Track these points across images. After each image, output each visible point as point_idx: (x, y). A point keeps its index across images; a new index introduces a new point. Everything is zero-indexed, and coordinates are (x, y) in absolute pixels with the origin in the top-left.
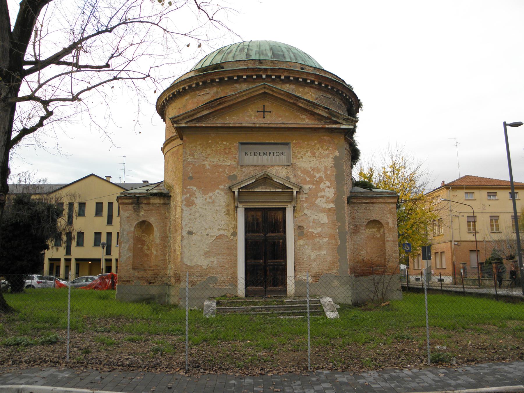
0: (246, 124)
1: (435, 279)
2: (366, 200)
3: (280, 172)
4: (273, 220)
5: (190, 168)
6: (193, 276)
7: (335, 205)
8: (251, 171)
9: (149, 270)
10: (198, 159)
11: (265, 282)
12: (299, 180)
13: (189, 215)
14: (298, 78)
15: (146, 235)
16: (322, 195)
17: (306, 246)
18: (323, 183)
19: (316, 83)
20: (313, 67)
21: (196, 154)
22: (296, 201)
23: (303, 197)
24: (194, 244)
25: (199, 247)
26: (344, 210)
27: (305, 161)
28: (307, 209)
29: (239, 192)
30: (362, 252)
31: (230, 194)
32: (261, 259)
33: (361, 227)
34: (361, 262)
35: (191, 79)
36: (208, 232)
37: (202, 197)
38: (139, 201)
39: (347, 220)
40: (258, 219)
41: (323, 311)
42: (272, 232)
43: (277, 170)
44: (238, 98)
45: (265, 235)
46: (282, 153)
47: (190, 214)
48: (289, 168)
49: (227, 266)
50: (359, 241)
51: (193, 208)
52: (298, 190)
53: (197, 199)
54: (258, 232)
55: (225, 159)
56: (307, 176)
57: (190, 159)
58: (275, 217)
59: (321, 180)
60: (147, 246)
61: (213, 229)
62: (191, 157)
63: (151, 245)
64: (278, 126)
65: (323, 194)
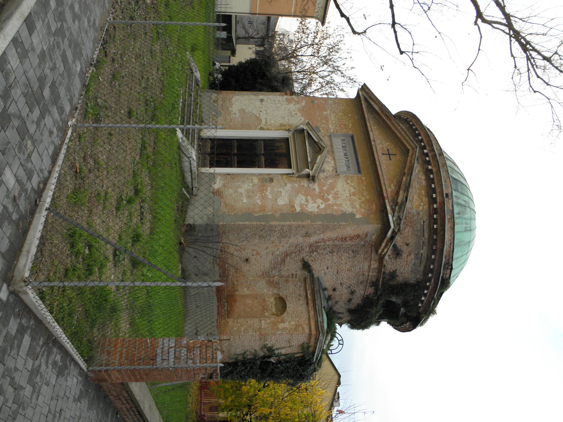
1: (219, 6)
2: (310, 295)
6: (222, 102)
7: (299, 212)
12: (322, 181)
17: (251, 185)
18: (323, 202)
20: (453, 210)
25: (250, 106)
30: (245, 289)
32: (238, 150)
33: (276, 289)
34: (233, 287)
42: (265, 161)
44: (397, 129)
45: (263, 154)
46: (349, 167)
48: (334, 172)
50: (259, 286)
54: (265, 150)
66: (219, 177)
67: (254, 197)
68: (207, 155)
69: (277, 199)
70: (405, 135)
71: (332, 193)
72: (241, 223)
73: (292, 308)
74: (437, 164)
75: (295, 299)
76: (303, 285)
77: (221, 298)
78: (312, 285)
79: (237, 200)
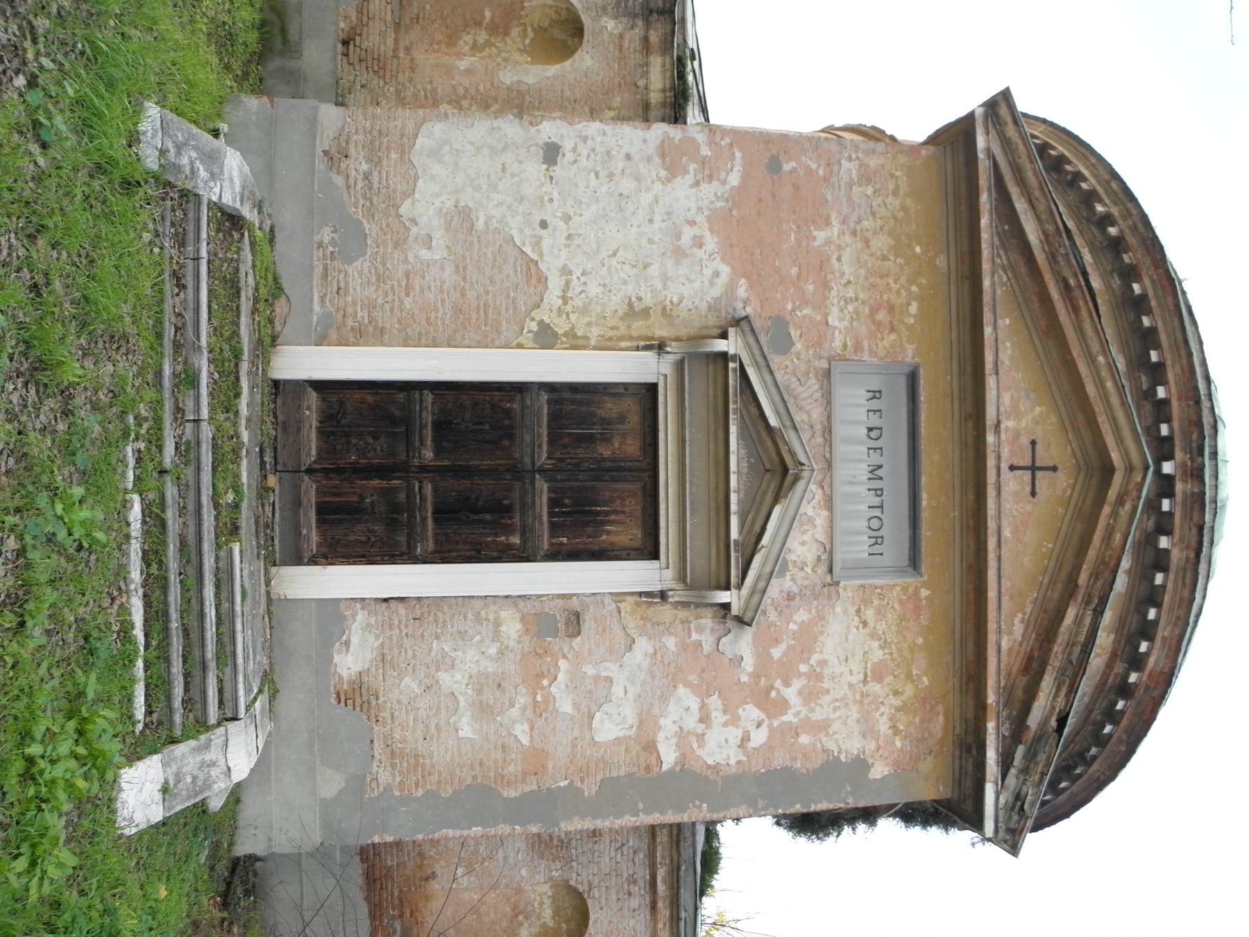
0: (994, 392)
2: (664, 882)
3: (804, 533)
4: (605, 503)
5: (814, 166)
6: (369, 160)
7: (671, 772)
8: (808, 412)
9: (396, 40)
10: (849, 198)
11: (339, 470)
12: (773, 616)
13: (625, 150)
14: (1158, 605)
15: (527, 41)
16: (714, 714)
17: (493, 651)
18: (763, 716)
19: (1133, 678)
21: (870, 191)
22: (685, 605)
23: (704, 631)
24: (504, 169)
25: (494, 187)
26: (647, 813)
27: (851, 637)
28: (651, 651)
29: (724, 356)
31: (712, 320)
32: (439, 450)
33: (559, 865)
34: (420, 867)
35: (1121, 196)
36: (555, 229)
37: (700, 209)
38: (655, 16)
39: (607, 823)
40: (607, 439)
41: (174, 741)
42: (553, 503)
43: (811, 520)
44: (1092, 360)
45: (542, 471)
46: (878, 540)
47: (628, 157)
48: (822, 569)
49: (408, 302)
51: (656, 170)
52: (735, 610)
53: (691, 187)
55: (850, 308)
56: (790, 648)
57: (849, 168)
58: (615, 512)
59: (773, 706)
60: (488, 44)
61: (568, 246)
62: (854, 172)
63: (490, 56)
64: (991, 524)
65: (718, 717)
66: (361, 616)
67: (502, 712)
68: (306, 478)
69: (591, 717)
70: (1115, 400)
71: (800, 675)
72: (451, 833)
73: (606, 922)
74: (1194, 540)
75: (618, 893)
76: (644, 845)
77: (380, 904)
78: (674, 852)
79: (438, 727)
